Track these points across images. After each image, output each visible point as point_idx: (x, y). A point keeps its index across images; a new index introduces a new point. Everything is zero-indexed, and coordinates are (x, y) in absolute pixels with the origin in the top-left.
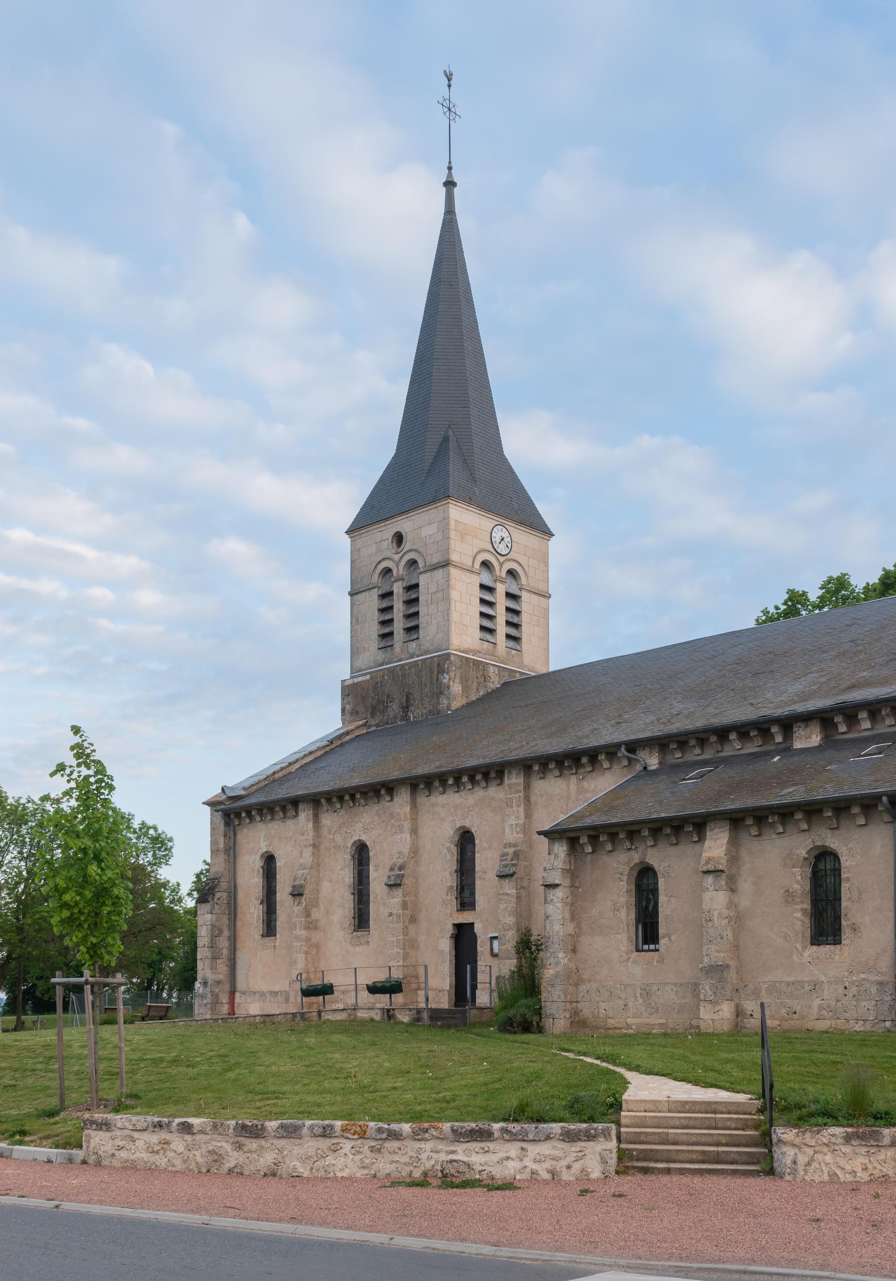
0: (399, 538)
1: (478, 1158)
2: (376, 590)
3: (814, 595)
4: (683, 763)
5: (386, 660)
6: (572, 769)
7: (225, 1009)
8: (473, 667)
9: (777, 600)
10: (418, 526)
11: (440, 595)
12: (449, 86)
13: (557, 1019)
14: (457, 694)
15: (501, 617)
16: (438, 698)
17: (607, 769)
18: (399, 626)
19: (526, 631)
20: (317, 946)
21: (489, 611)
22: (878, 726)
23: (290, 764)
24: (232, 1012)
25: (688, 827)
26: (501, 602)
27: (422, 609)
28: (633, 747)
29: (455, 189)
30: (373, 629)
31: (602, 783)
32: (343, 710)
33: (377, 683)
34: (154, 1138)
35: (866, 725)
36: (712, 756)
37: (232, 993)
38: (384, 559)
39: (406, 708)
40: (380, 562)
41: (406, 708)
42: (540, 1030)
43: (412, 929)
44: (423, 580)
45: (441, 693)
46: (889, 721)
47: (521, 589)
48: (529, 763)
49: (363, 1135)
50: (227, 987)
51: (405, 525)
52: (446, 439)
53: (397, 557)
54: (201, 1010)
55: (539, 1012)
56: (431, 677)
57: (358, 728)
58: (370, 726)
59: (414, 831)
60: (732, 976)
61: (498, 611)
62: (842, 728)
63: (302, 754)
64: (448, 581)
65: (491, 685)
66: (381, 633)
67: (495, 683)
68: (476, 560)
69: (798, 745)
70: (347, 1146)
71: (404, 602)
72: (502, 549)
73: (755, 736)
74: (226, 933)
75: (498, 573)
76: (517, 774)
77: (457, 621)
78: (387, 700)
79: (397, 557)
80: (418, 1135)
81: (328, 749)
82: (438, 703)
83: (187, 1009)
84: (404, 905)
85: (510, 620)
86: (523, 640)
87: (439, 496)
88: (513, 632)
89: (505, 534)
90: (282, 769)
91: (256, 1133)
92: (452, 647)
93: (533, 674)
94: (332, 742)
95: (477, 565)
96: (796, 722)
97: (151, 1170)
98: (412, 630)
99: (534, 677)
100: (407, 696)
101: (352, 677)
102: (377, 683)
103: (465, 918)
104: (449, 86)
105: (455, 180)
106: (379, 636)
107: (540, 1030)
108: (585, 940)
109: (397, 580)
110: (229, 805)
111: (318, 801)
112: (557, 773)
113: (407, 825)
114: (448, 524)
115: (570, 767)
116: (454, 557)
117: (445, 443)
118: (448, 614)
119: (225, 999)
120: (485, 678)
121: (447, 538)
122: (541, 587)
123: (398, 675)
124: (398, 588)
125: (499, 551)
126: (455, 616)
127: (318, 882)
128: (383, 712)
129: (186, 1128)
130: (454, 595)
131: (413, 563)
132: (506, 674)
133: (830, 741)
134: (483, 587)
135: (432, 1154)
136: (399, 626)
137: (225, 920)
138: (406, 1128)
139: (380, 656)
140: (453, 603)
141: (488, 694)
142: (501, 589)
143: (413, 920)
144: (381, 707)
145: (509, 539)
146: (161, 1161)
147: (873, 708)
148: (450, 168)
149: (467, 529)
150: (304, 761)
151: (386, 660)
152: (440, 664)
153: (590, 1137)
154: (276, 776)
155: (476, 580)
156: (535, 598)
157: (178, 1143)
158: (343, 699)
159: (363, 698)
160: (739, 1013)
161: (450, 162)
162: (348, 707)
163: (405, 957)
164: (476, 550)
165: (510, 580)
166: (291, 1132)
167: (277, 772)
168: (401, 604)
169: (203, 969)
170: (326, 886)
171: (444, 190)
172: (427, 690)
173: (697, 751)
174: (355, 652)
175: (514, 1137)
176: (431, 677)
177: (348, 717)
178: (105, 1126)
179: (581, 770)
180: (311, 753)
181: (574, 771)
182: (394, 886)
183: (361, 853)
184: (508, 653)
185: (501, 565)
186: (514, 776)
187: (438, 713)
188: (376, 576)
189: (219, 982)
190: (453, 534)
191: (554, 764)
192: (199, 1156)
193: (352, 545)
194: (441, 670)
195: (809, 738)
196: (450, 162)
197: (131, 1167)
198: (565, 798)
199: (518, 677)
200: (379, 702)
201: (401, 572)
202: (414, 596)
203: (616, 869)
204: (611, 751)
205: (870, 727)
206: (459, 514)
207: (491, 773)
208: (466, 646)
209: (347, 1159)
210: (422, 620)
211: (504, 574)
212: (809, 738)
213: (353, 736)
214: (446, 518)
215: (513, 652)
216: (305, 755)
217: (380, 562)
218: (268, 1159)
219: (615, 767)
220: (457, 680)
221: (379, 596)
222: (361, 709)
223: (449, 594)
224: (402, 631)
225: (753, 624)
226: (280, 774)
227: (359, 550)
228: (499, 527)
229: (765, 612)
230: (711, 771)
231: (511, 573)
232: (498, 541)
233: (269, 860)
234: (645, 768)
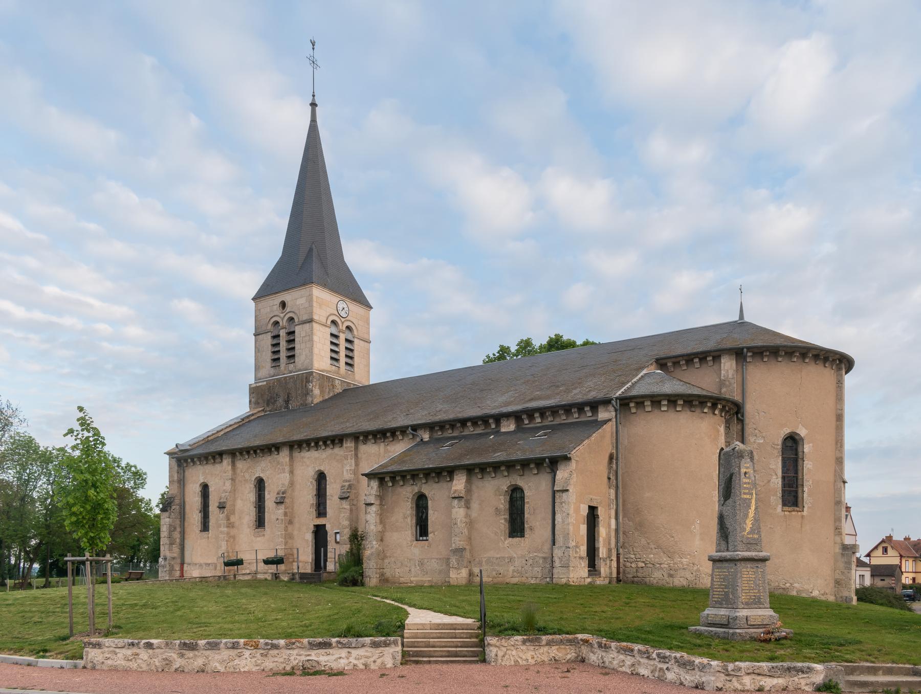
0: (283, 305)
1: (323, 658)
3: (513, 349)
7: (178, 574)
9: (494, 351)
10: (295, 298)
11: (307, 338)
13: (372, 578)
14: (317, 395)
15: (343, 352)
18: (283, 355)
20: (234, 537)
21: (336, 349)
24: (182, 575)
25: (444, 473)
26: (343, 344)
27: (297, 346)
28: (415, 428)
30: (268, 356)
31: (398, 448)
34: (129, 652)
35: (539, 420)
37: (182, 564)
39: (287, 402)
41: (287, 402)
42: (363, 584)
43: (290, 528)
49: (256, 647)
50: (179, 561)
51: (287, 297)
53: (282, 315)
54: (163, 575)
55: (362, 575)
59: (291, 472)
60: (467, 554)
62: (526, 422)
67: (339, 389)
69: (503, 430)
70: (247, 653)
72: (343, 314)
74: (178, 529)
77: (317, 354)
79: (282, 315)
80: (288, 647)
83: (155, 573)
84: (285, 514)
87: (307, 282)
88: (349, 361)
89: (345, 306)
91: (192, 647)
95: (329, 322)
97: (127, 671)
98: (291, 357)
103: (320, 521)
107: (363, 584)
108: (387, 534)
110: (180, 455)
111: (234, 454)
113: (287, 469)
114: (312, 298)
115: (380, 438)
116: (316, 317)
117: (310, 252)
119: (177, 568)
120: (333, 386)
122: (365, 336)
123: (283, 383)
124: (283, 333)
126: (316, 351)
127: (235, 500)
128: (273, 404)
129: (149, 646)
130: (315, 338)
133: (520, 428)
134: (332, 335)
135: (297, 656)
136: (283, 355)
137: (178, 522)
138: (282, 642)
139: (272, 371)
142: (342, 337)
143: (291, 522)
146: (133, 665)
149: (322, 302)
152: (307, 377)
153: (386, 645)
157: (144, 655)
159: (262, 395)
160: (471, 574)
163: (286, 543)
165: (347, 332)
166: (213, 646)
169: (164, 551)
170: (239, 504)
173: (450, 431)
174: (257, 368)
175: (344, 646)
178: (98, 645)
182: (279, 503)
183: (260, 484)
189: (174, 558)
190: (315, 304)
192: (157, 662)
194: (308, 381)
195: (509, 426)
197: (114, 669)
198: (377, 456)
199: (352, 386)
200: (271, 397)
203: (406, 494)
204: (403, 430)
206: (318, 293)
207: (336, 440)
208: (322, 368)
209: (247, 661)
210: (297, 352)
212: (509, 426)
214: (311, 295)
218: (199, 662)
225: (481, 363)
229: (488, 357)
231: (348, 328)
233: (205, 488)
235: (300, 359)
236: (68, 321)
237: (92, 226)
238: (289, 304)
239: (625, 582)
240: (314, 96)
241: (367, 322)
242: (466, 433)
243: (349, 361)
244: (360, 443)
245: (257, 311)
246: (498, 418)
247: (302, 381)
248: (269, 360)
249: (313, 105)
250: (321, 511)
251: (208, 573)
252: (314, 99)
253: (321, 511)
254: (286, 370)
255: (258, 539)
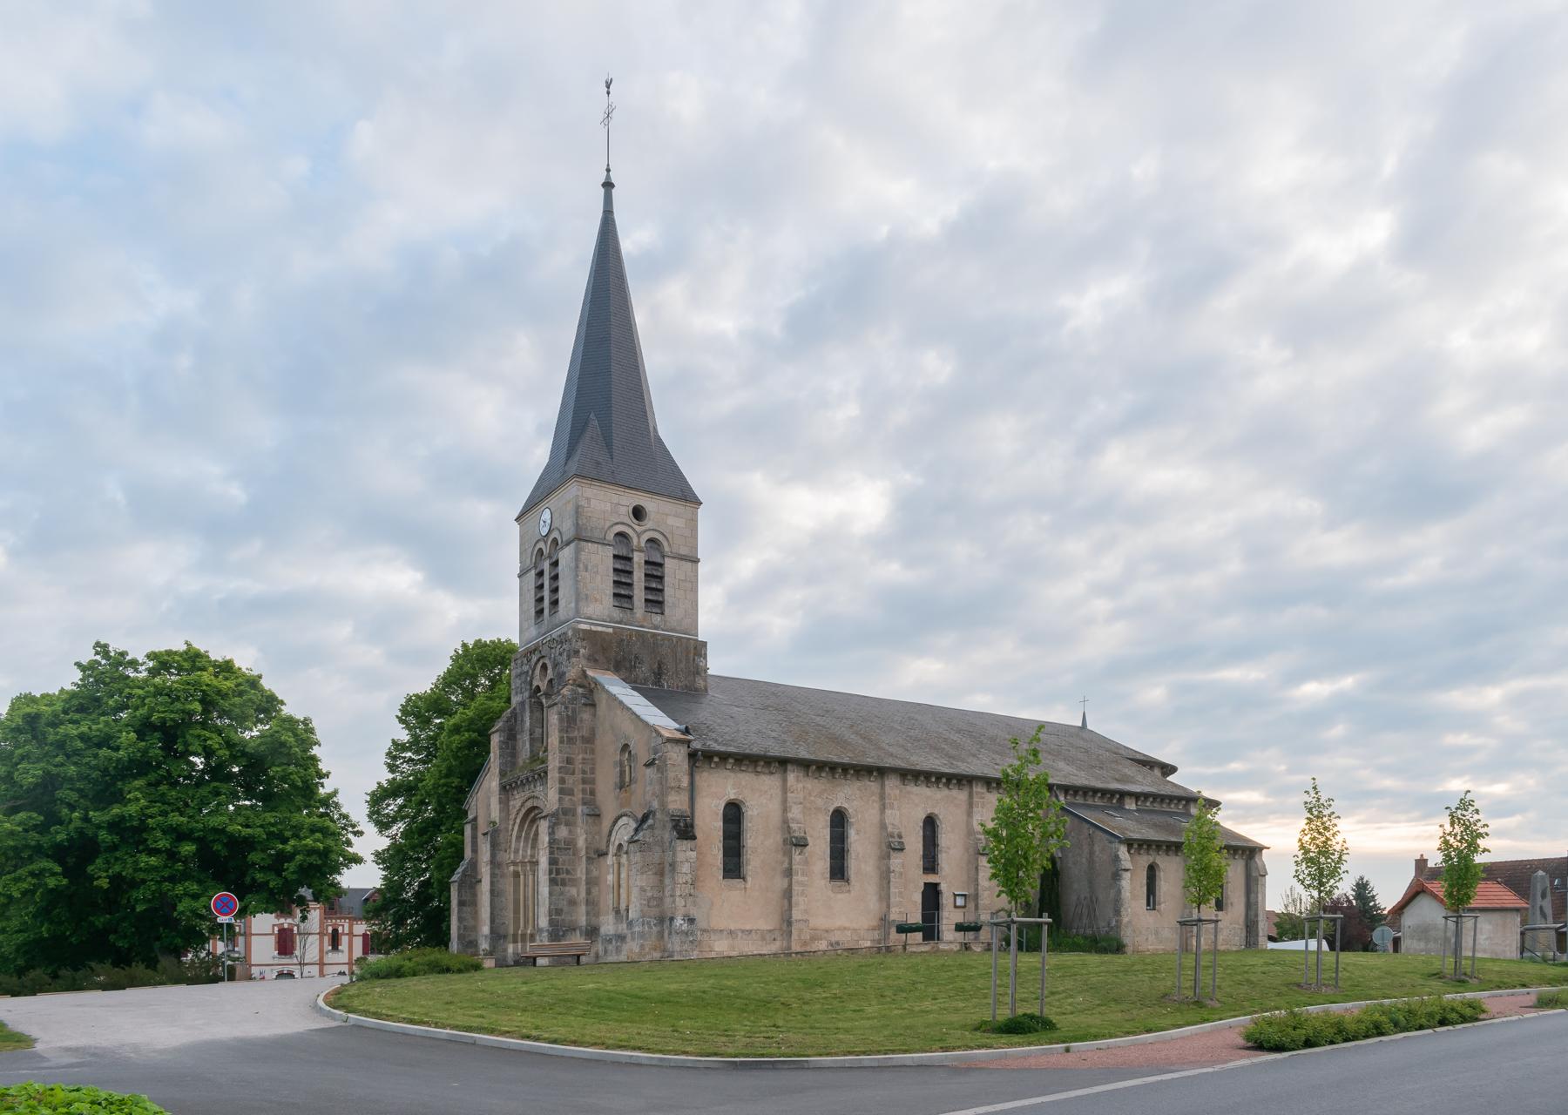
103: (932, 879)
136: (639, 594)
139: (617, 614)
239: (661, 935)
240: (608, 170)
242: (1090, 802)
247: (688, 653)
250: (930, 865)
251: (750, 947)
252: (608, 176)
253: (930, 865)
255: (840, 896)
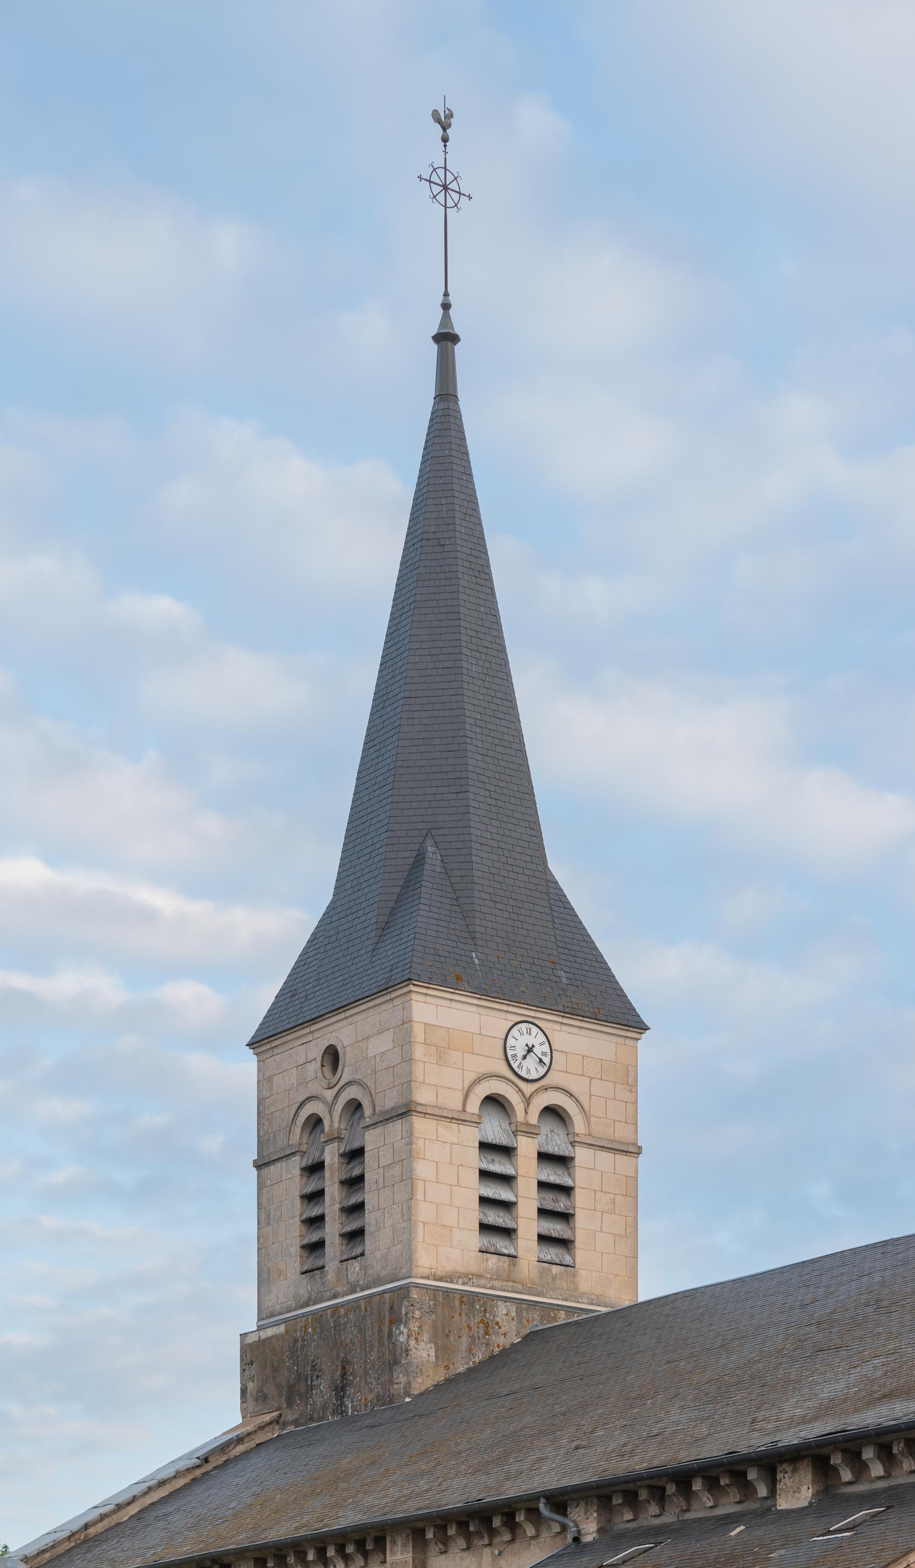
0: (332, 1056)
2: (297, 1158)
4: (634, 1530)
5: (314, 1295)
6: (482, 1537)
8: (458, 1305)
11: (397, 1171)
12: (445, 140)
14: (424, 1360)
15: (528, 1199)
16: (391, 1372)
17: (532, 1538)
18: (332, 1230)
19: (584, 1225)
21: (503, 1194)
22: (895, 1472)
23: (119, 1507)
26: (528, 1170)
28: (560, 1501)
29: (458, 348)
30: (293, 1235)
32: (244, 1392)
33: (296, 1341)
35: (877, 1469)
36: (675, 1519)
38: (309, 1099)
39: (340, 1390)
40: (302, 1104)
41: (340, 1390)
44: (371, 1141)
45: (396, 1362)
46: (907, 1464)
47: (573, 1143)
48: (420, 1525)
51: (341, 1032)
52: (420, 859)
53: (329, 1095)
56: (380, 1330)
57: (261, 1428)
58: (285, 1425)
61: (521, 1192)
62: (846, 1475)
63: (144, 1487)
64: (410, 1143)
65: (501, 1341)
66: (305, 1242)
67: (508, 1333)
68: (472, 1097)
69: (784, 1503)
71: (342, 1183)
72: (531, 1068)
73: (727, 1485)
75: (520, 1116)
76: (404, 1546)
77: (436, 1222)
78: (306, 1373)
79: (329, 1095)
81: (198, 1472)
82: (391, 1382)
85: (549, 1206)
86: (578, 1244)
87: (393, 983)
88: (555, 1228)
89: (536, 1039)
90: (102, 1517)
92: (420, 1271)
93: (604, 1310)
94: (206, 1460)
95: (474, 1106)
96: (781, 1463)
98: (355, 1236)
99: (608, 1313)
100: (343, 1368)
101: (260, 1328)
102: (296, 1341)
104: (445, 140)
105: (457, 330)
106: (303, 1247)
109: (329, 1141)
112: (461, 1543)
114: (409, 1033)
115: (479, 1534)
116: (423, 1096)
117: (440, 860)
118: (409, 1207)
121: (408, 1060)
122: (622, 1133)
124: (331, 1156)
125: (523, 1073)
126: (423, 1212)
128: (305, 1397)
130: (422, 1169)
131: (355, 1107)
132: (536, 1315)
133: (830, 1496)
134: (485, 1147)
136: (332, 1230)
139: (304, 1286)
140: (420, 1186)
141: (492, 1358)
142: (527, 1148)
144: (302, 1388)
145: (546, 1048)
147: (884, 1441)
148: (446, 306)
149: (451, 1040)
150: (148, 1500)
151: (314, 1295)
152: (391, 1309)
154: (92, 1531)
155: (471, 1136)
156: (605, 1158)
158: (243, 1371)
159: (276, 1370)
161: (446, 294)
162: (251, 1386)
164: (470, 1077)
165: (548, 1128)
167: (94, 1523)
168: (337, 1186)
171: (435, 347)
172: (373, 1356)
173: (654, 1509)
174: (265, 1278)
176: (380, 1330)
177: (251, 1405)
179: (497, 1540)
180: (162, 1483)
181: (486, 1541)
184: (542, 1274)
185: (528, 1101)
186: (399, 1548)
187: (391, 1402)
188: (297, 1130)
190: (419, 1052)
191: (454, 1527)
193: (259, 1070)
194: (396, 1320)
195: (797, 1492)
196: (446, 294)
199: (562, 1318)
200: (299, 1377)
201: (336, 1125)
202: (356, 1172)
204: (528, 1506)
205: (882, 1473)
206: (432, 1011)
208: (447, 1267)
210: (370, 1218)
211: (534, 1118)
212: (797, 1492)
213: (252, 1444)
214: (407, 1022)
215: (555, 1269)
216: (150, 1489)
217: (302, 1104)
219: (545, 1535)
220: (426, 1337)
221: (303, 1169)
222: (271, 1390)
223: (411, 1170)
224: (337, 1239)
226: (100, 1527)
227: (270, 1080)
228: (523, 1026)
230: (652, 1548)
231: (553, 1112)
232: (521, 1052)
234: (576, 1540)
235: (377, 1244)
236: (65, 984)
237: (160, 608)
238: (347, 1057)
241: (627, 1077)
243: (555, 1228)
244: (434, 1549)
245: (264, 1081)
246: (772, 1463)
248: (295, 1249)
249: (446, 339)
252: (446, 319)
254: (346, 1283)
